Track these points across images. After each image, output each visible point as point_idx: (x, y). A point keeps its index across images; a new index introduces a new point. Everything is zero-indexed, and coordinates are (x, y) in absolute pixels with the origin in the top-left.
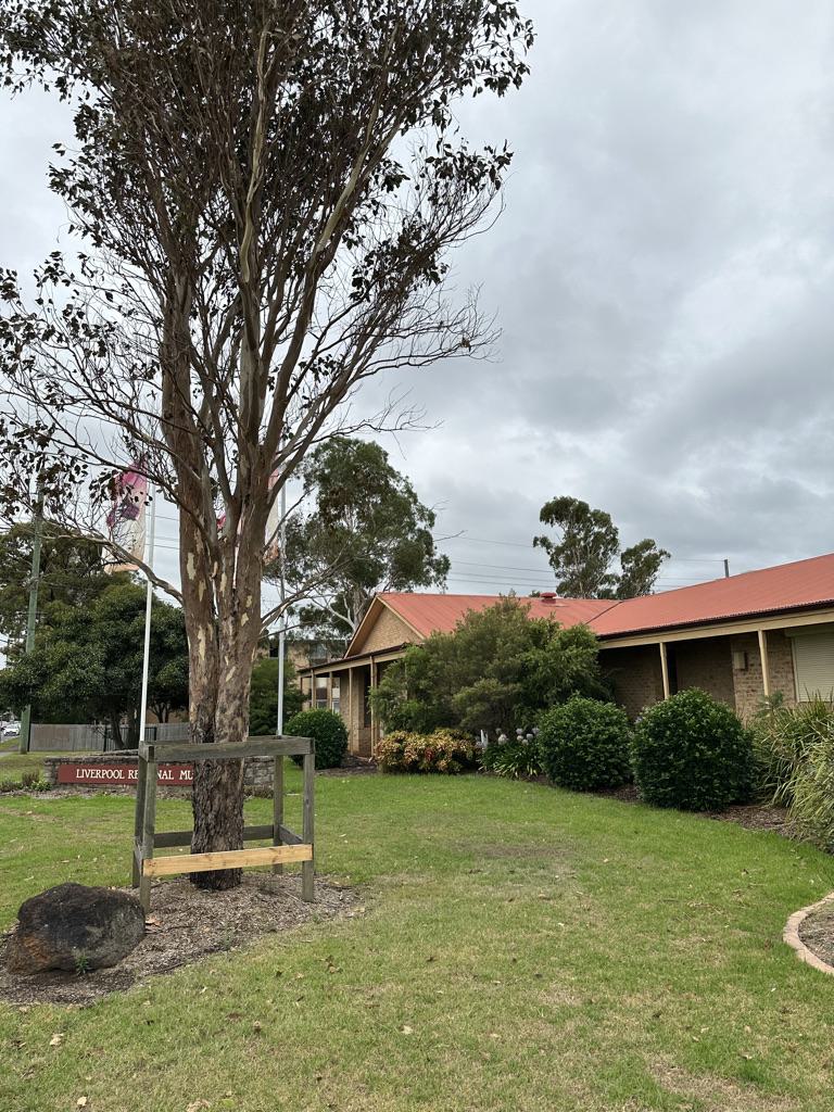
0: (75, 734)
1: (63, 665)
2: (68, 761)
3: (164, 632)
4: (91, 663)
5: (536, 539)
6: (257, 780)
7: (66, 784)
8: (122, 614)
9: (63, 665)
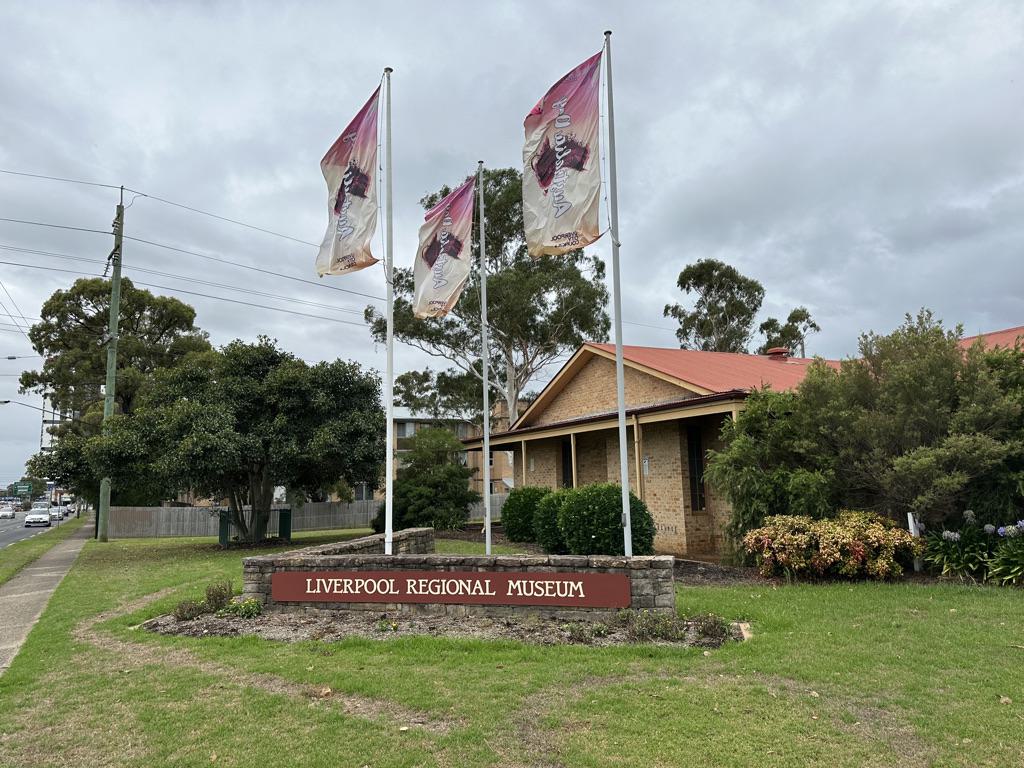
0: (158, 519)
1: (183, 429)
2: (287, 566)
3: (308, 390)
4: (221, 427)
5: (667, 308)
6: (663, 600)
7: (286, 603)
8: (248, 369)
9: (183, 429)
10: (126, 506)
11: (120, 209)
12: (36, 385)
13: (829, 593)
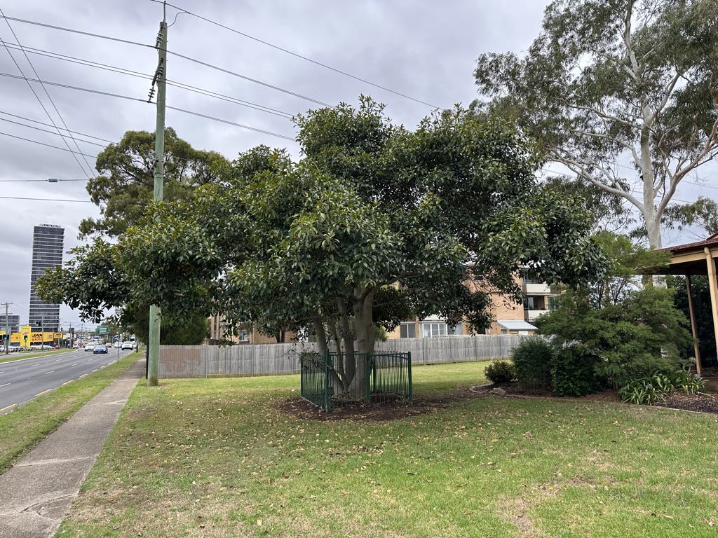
10: (174, 344)
11: (163, 26)
12: (93, 232)
13: (430, 366)
